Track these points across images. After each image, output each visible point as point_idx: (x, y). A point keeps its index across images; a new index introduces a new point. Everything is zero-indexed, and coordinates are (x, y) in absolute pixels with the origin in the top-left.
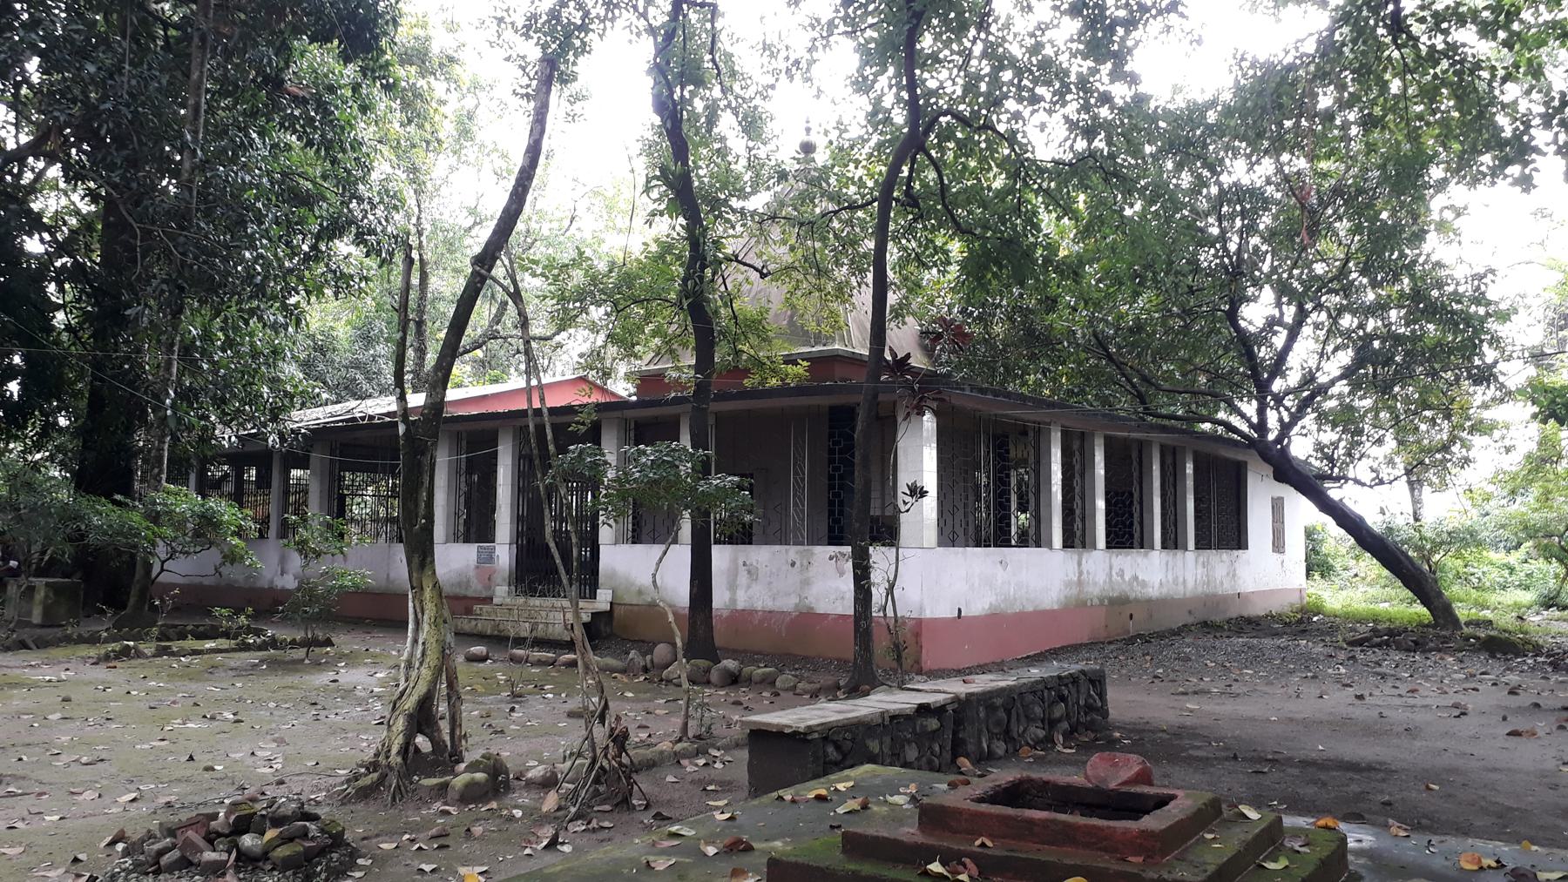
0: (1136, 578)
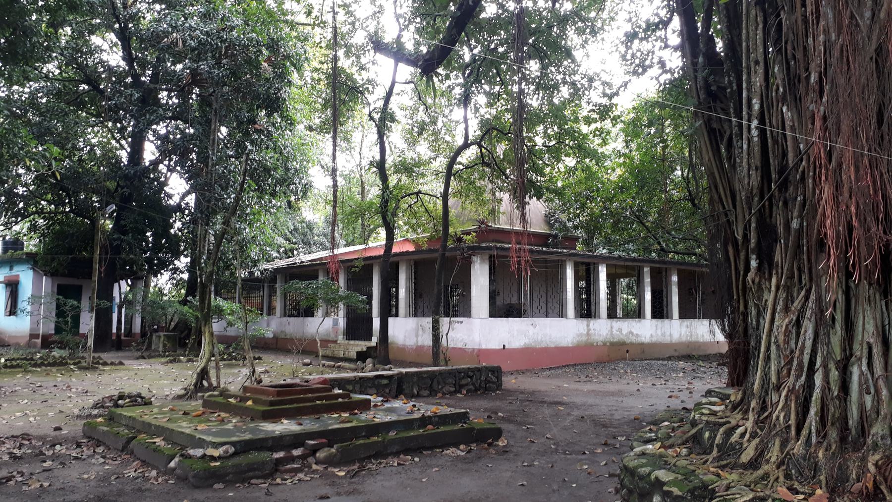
0: (631, 333)
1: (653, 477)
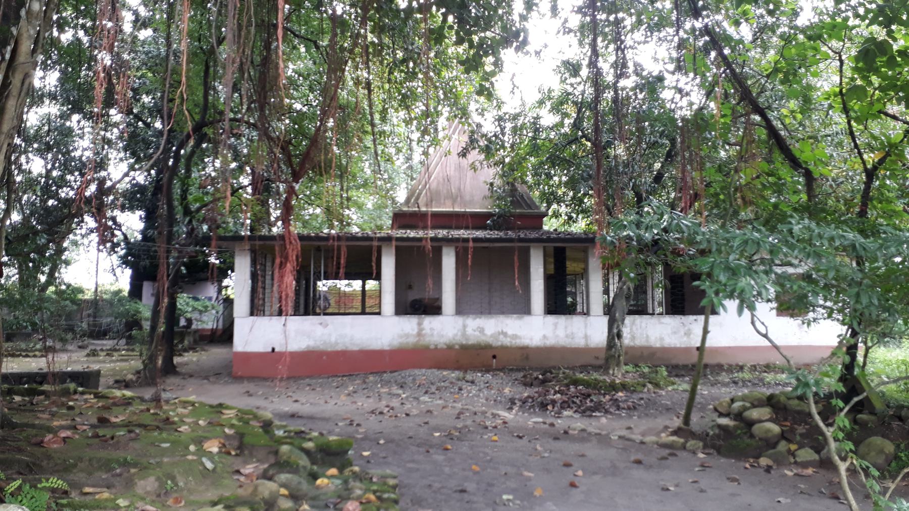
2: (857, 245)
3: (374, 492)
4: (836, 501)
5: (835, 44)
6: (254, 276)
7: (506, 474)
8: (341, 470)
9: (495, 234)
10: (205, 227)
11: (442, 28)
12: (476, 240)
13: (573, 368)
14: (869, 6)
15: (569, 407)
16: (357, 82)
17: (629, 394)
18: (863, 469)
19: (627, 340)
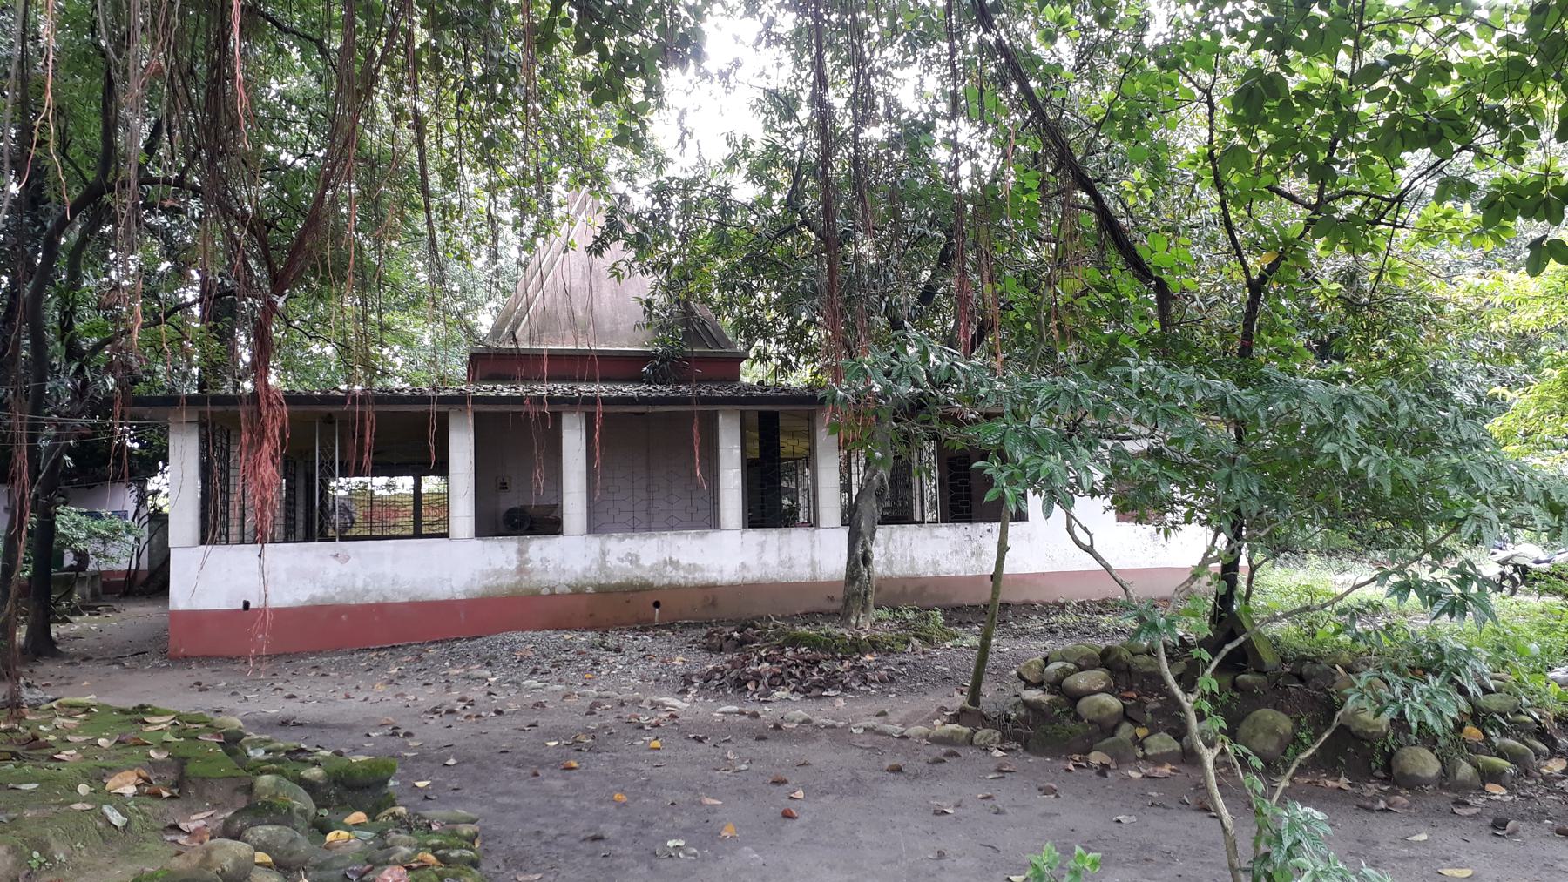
1: (1348, 691)
2: (1229, 400)
3: (434, 849)
4: (1205, 814)
5: (1204, 77)
6: (206, 471)
7: (673, 804)
8: (372, 815)
9: (658, 390)
10: (111, 381)
11: (550, 23)
12: (606, 401)
13: (791, 618)
14: (1250, 18)
15: (783, 683)
16: (398, 114)
17: (881, 657)
18: (1239, 759)
19: (879, 567)
